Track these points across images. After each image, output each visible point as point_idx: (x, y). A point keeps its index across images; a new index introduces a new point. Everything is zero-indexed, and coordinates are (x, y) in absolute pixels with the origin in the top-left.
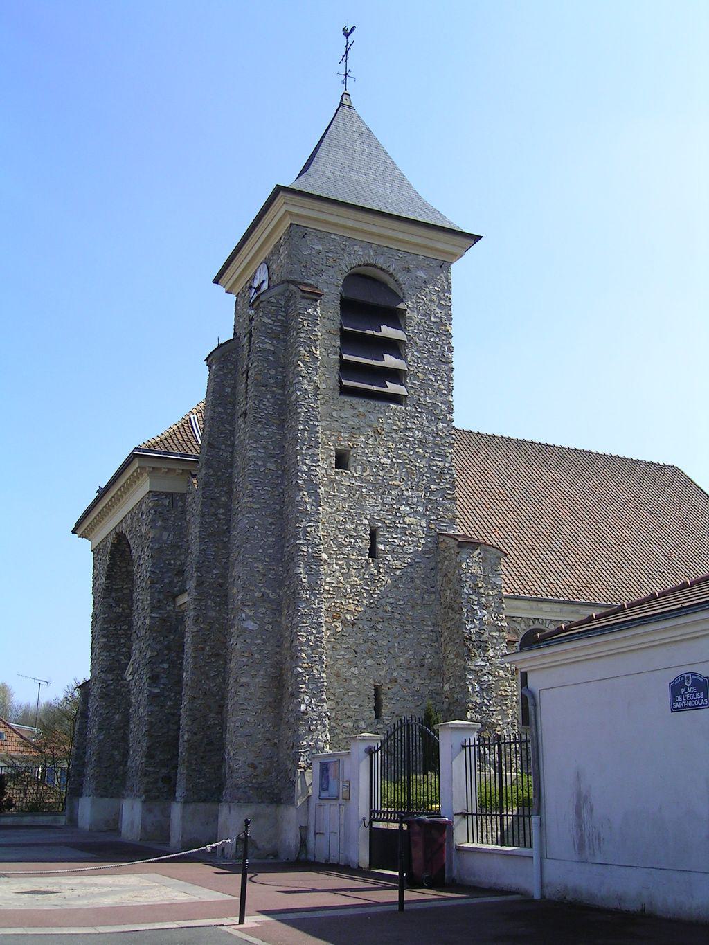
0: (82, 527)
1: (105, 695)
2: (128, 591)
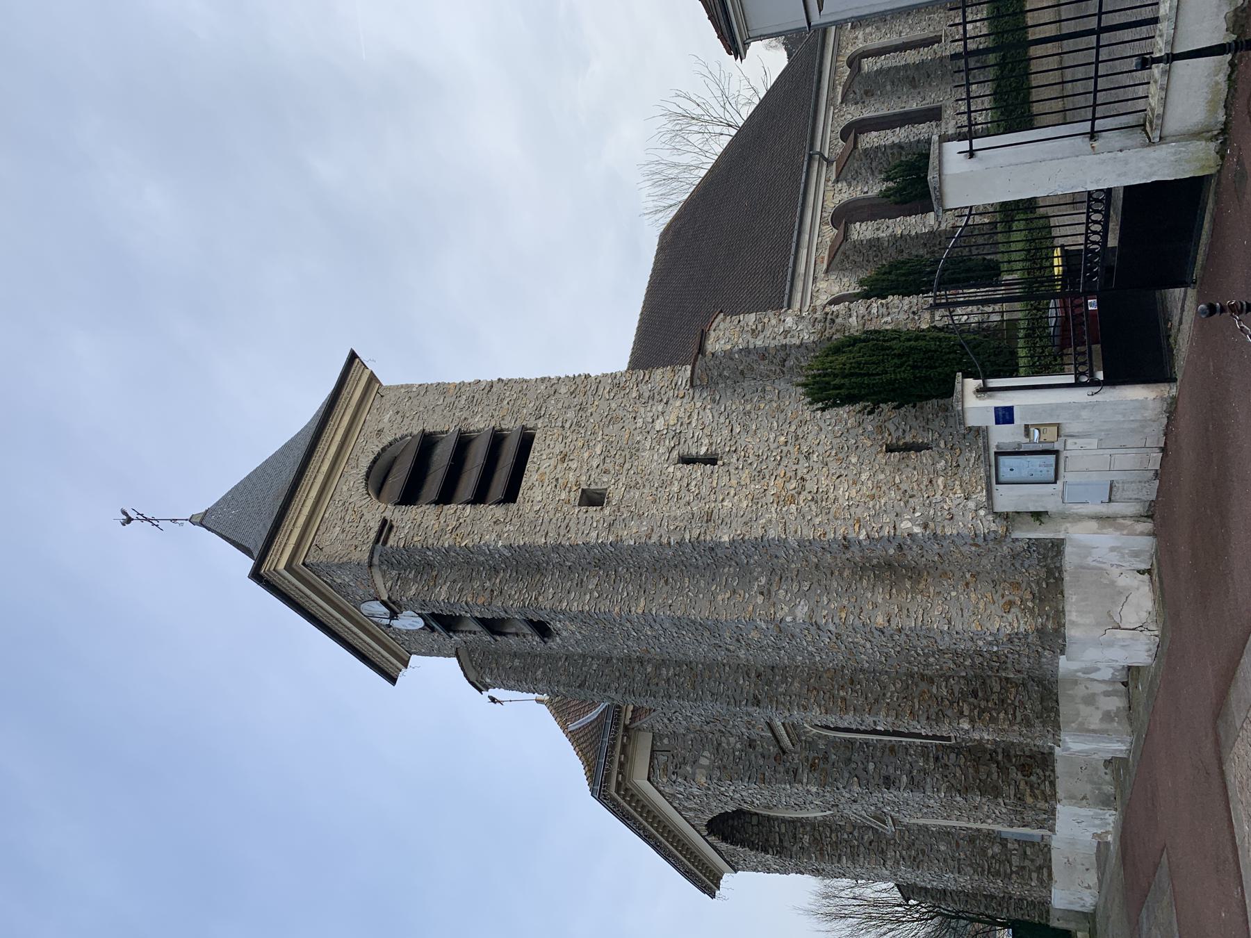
0: (708, 882)
1: (915, 863)
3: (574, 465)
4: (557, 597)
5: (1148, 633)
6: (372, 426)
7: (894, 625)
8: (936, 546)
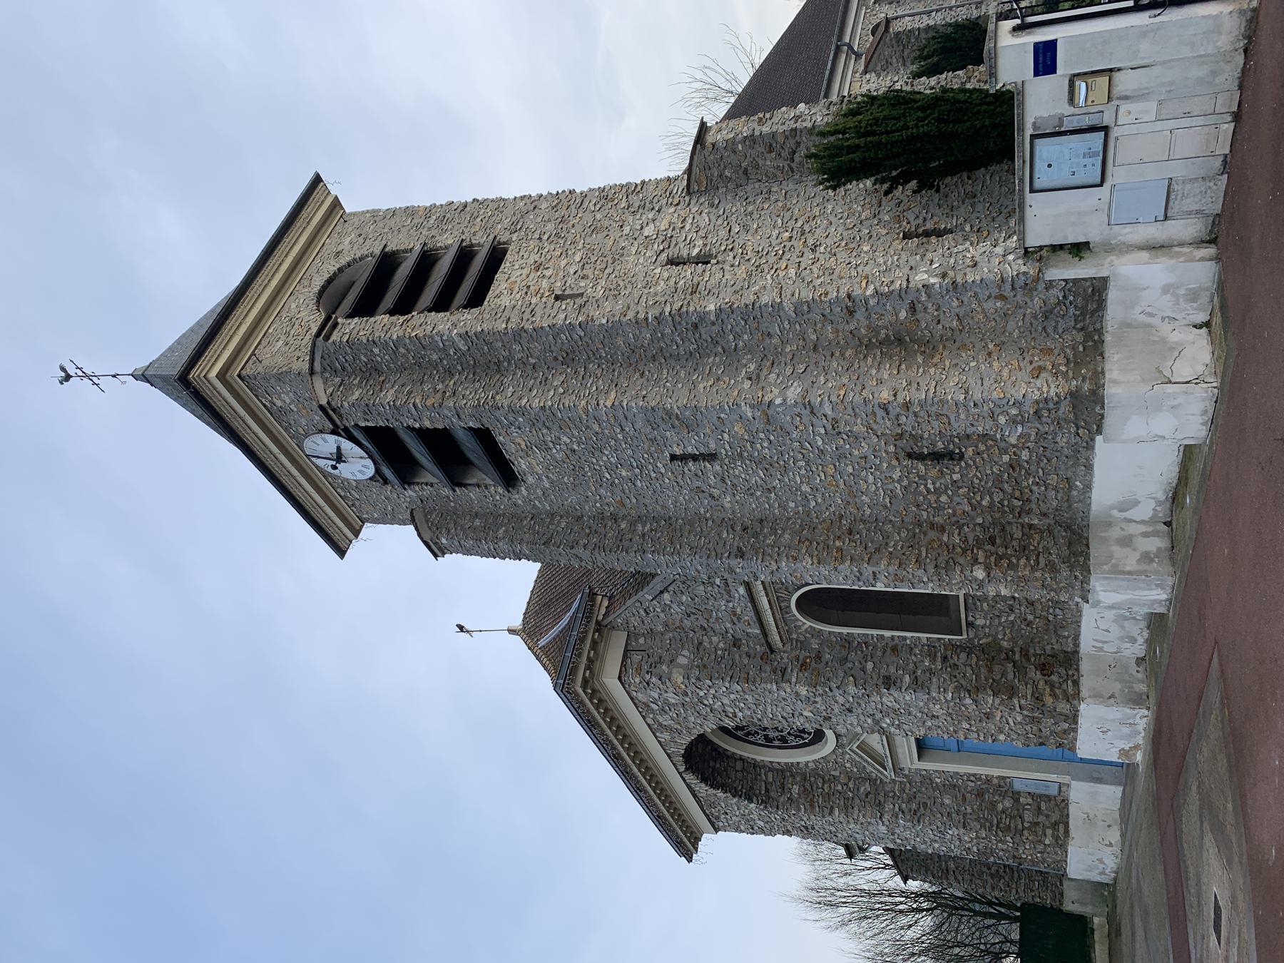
1: (916, 816)
2: (770, 774)
3: (548, 273)
4: (516, 395)
5: (1205, 385)
6: (331, 247)
7: (900, 399)
8: (955, 303)
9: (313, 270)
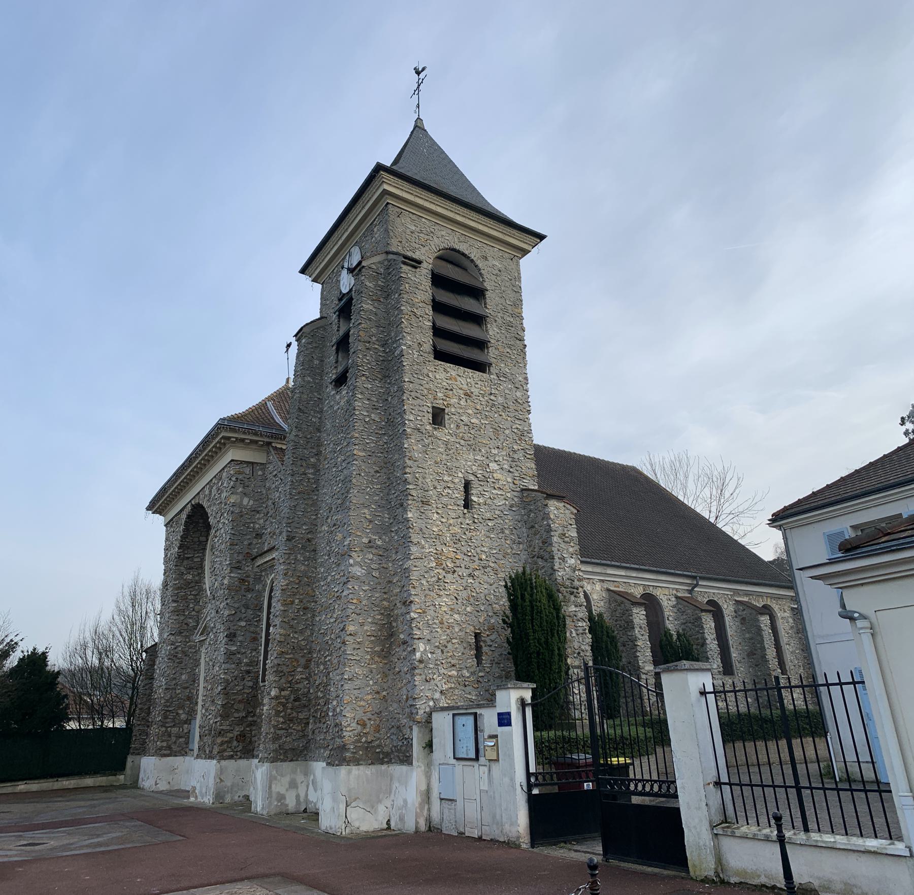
1: (173, 657)
3: (463, 402)
4: (364, 390)
6: (490, 252)
7: (347, 638)
8: (406, 669)
9: (472, 242)
